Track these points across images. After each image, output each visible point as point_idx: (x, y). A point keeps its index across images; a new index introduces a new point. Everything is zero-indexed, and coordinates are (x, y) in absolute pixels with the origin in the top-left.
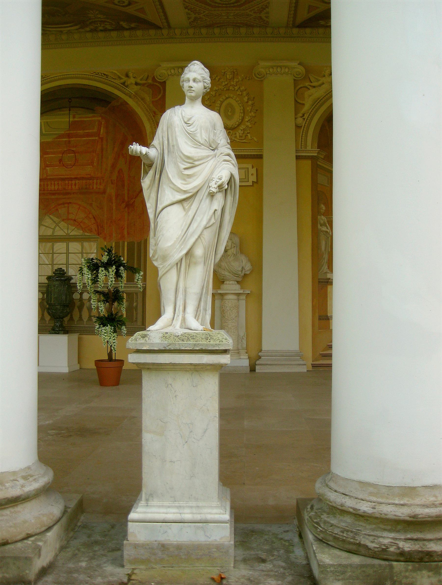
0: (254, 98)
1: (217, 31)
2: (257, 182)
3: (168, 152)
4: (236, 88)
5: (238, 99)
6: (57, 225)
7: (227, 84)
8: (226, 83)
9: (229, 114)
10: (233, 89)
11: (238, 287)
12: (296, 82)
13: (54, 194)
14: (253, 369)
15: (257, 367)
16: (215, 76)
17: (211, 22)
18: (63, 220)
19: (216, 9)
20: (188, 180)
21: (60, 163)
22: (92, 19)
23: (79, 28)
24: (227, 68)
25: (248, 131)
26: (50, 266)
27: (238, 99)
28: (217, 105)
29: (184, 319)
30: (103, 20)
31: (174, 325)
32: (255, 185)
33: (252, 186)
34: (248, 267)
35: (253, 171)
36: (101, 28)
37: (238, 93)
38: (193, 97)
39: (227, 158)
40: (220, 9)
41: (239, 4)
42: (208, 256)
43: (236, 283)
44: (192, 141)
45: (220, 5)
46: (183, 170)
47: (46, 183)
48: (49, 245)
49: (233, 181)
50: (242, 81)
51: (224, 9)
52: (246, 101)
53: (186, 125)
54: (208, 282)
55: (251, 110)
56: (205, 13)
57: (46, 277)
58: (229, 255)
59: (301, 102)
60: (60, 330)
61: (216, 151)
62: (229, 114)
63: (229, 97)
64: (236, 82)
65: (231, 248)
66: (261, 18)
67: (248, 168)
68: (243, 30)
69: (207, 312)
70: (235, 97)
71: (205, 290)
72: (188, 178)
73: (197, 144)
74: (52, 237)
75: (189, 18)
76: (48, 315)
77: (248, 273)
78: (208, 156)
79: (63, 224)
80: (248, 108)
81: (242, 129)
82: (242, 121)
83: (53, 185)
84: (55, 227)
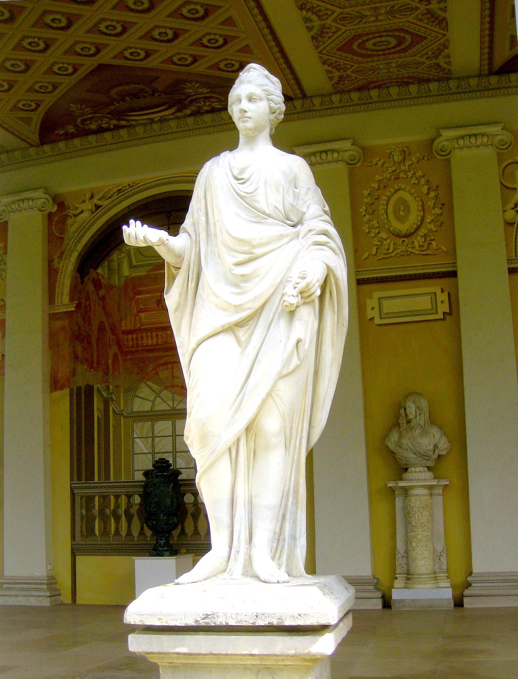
0: (437, 187)
1: (374, 93)
2: (450, 314)
3: (208, 236)
4: (410, 174)
5: (413, 191)
6: (158, 395)
7: (396, 170)
8: (394, 168)
9: (402, 213)
10: (405, 176)
11: (430, 475)
12: (500, 158)
13: (151, 351)
14: (459, 603)
15: (466, 600)
16: (377, 160)
17: (365, 81)
18: (166, 388)
19: (369, 59)
20: (243, 285)
21: (158, 305)
22: (192, 96)
23: (176, 112)
24: (394, 147)
25: (432, 238)
26: (150, 456)
27: (413, 191)
28: (382, 202)
29: (250, 558)
30: (208, 95)
31: (230, 570)
32: (448, 317)
33: (444, 319)
34: (444, 445)
35: (444, 297)
36: (206, 108)
37: (413, 181)
38: (250, 130)
39: (323, 239)
40: (376, 58)
41: (403, 47)
42: (294, 432)
43: (426, 469)
44: (249, 211)
45: (375, 53)
46: (233, 267)
47: (139, 336)
48: (148, 424)
49: (333, 281)
50: (418, 162)
51: (382, 58)
52: (426, 192)
53: (237, 182)
54: (297, 482)
55: (434, 205)
56: (353, 68)
57: (142, 472)
58: (413, 428)
59: (511, 186)
60: (164, 551)
61: (299, 227)
62: (402, 213)
63: (399, 190)
64: (409, 166)
65: (416, 417)
66: (438, 65)
67: (435, 293)
68: (413, 89)
69: (298, 542)
70: (408, 187)
71: (291, 498)
72: (245, 281)
73: (259, 216)
74: (150, 414)
75: (331, 79)
76: (147, 528)
77: (444, 453)
78: (281, 237)
79: (166, 394)
80: (429, 203)
81: (422, 234)
82: (421, 223)
83: (149, 338)
84: (155, 398)
